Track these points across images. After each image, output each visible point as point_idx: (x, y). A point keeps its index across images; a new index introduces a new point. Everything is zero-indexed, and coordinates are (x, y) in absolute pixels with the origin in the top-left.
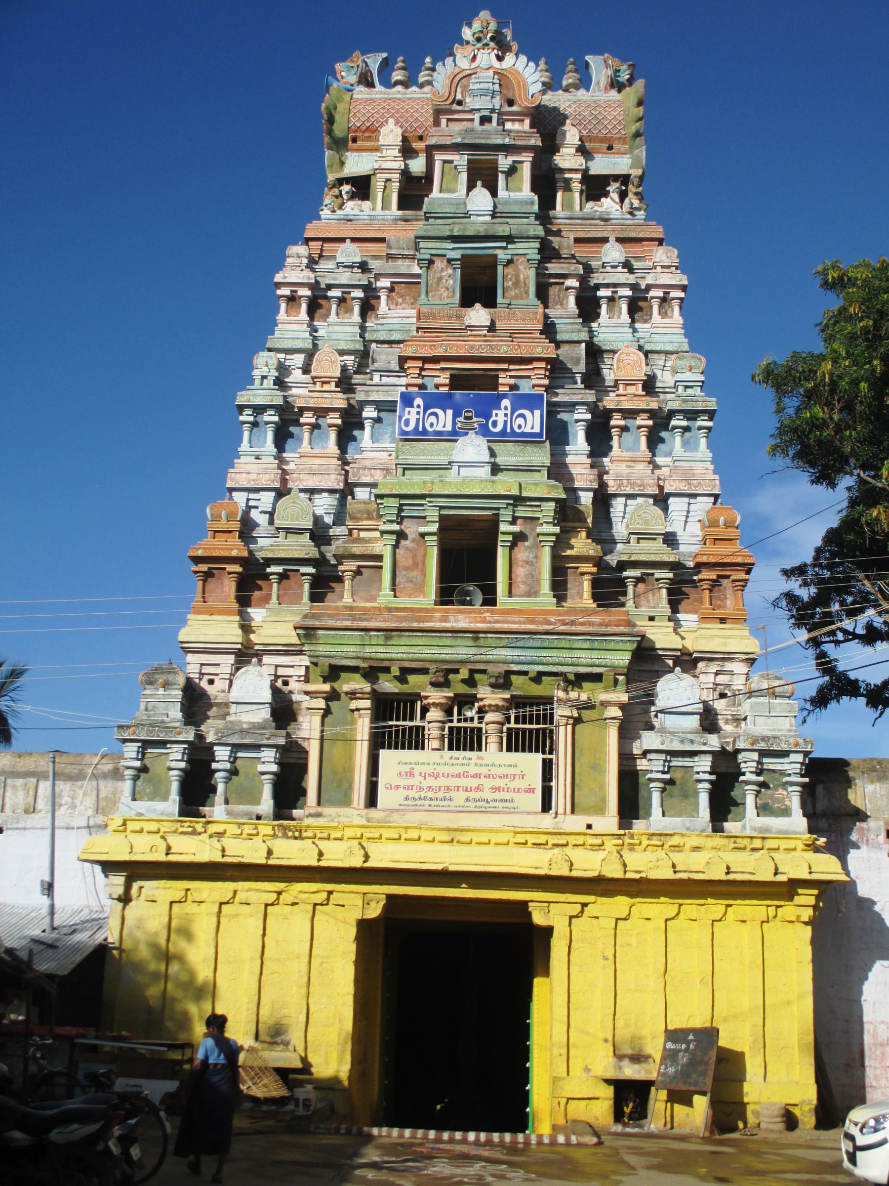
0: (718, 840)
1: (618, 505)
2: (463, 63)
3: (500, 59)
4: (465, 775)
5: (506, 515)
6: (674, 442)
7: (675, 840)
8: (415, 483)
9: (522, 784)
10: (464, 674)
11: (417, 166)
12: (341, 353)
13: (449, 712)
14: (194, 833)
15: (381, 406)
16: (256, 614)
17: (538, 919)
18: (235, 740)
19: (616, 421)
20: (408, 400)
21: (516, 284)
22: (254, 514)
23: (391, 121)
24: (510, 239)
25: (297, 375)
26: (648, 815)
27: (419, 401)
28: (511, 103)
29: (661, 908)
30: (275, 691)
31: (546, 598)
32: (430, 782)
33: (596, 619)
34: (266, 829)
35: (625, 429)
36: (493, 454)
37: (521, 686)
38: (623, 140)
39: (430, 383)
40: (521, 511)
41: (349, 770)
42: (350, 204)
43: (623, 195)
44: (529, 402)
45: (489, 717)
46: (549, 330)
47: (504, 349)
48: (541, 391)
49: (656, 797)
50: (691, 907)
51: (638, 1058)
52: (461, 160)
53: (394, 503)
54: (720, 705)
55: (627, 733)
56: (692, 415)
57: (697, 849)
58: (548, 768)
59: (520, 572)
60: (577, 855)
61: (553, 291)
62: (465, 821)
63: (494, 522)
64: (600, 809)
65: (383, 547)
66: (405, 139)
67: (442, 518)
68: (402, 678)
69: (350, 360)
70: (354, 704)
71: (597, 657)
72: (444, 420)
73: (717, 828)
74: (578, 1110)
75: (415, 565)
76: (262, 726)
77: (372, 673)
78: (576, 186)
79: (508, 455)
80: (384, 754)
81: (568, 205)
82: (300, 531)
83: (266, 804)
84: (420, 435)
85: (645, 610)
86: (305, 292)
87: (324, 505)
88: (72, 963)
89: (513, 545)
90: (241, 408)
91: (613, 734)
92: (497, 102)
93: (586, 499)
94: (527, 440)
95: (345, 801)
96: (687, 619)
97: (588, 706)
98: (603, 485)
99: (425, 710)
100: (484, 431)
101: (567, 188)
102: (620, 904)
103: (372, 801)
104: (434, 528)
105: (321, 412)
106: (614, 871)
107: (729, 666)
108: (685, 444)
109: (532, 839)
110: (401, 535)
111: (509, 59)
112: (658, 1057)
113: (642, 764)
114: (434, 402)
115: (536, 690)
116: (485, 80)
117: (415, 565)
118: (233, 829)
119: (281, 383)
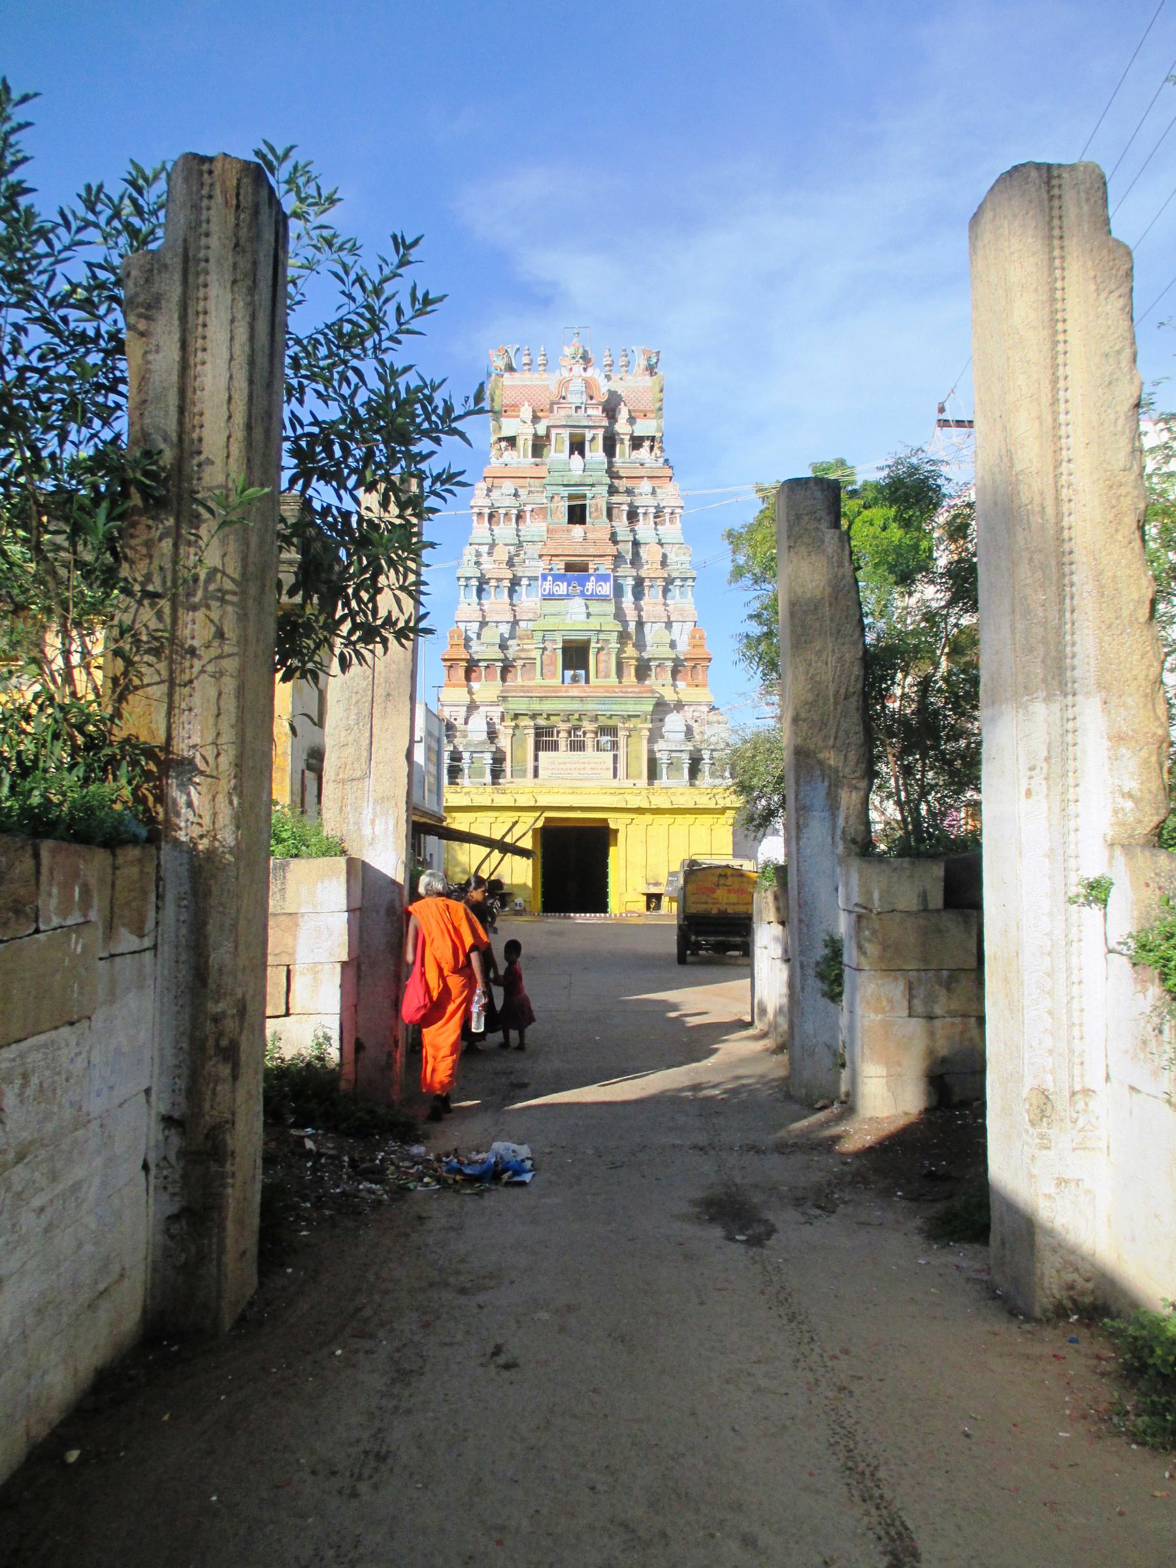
0: (693, 790)
1: (647, 628)
2: (566, 374)
3: (585, 370)
4: (578, 763)
5: (594, 639)
6: (675, 591)
7: (673, 790)
8: (549, 623)
9: (605, 766)
10: (576, 716)
11: (542, 431)
12: (506, 545)
13: (569, 733)
14: (456, 792)
15: (530, 578)
16: (475, 685)
17: (612, 826)
18: (472, 749)
19: (647, 583)
20: (544, 577)
21: (596, 510)
22: (469, 633)
23: (526, 404)
24: (593, 485)
25: (485, 558)
26: (661, 778)
27: (550, 578)
28: (591, 398)
29: (667, 819)
30: (488, 723)
31: (613, 679)
32: (562, 766)
33: (637, 690)
34: (489, 789)
35: (652, 586)
36: (587, 607)
37: (603, 721)
38: (652, 412)
39: (555, 567)
40: (602, 636)
41: (525, 761)
42: (506, 453)
43: (652, 448)
44: (603, 578)
45: (588, 735)
46: (614, 539)
47: (591, 551)
48: (609, 572)
49: (664, 771)
50: (680, 818)
51: (656, 884)
52: (565, 434)
53: (541, 634)
54: (695, 725)
55: (651, 740)
56: (684, 579)
57: (682, 794)
58: (615, 757)
59: (602, 666)
60: (628, 797)
61: (615, 512)
62: (578, 784)
63: (588, 642)
64: (639, 776)
65: (536, 654)
66: (534, 411)
67: (564, 642)
68: (548, 718)
69: (512, 549)
70: (526, 731)
71: (638, 707)
72: (562, 588)
73: (692, 785)
74: (630, 907)
75: (552, 663)
76: (483, 743)
77: (534, 717)
78: (627, 443)
79: (595, 607)
80: (541, 754)
81: (622, 455)
82: (494, 645)
83: (488, 778)
84: (549, 597)
85: (660, 682)
86: (487, 511)
87: (505, 629)
88: (760, 912)
89: (598, 653)
90: (459, 579)
91: (645, 743)
92: (584, 398)
93: (632, 627)
94: (604, 599)
95: (523, 773)
96: (681, 684)
97: (635, 729)
98: (640, 617)
99: (558, 732)
100: (582, 594)
101: (622, 441)
102: (648, 817)
103: (536, 775)
104: (560, 645)
105: (499, 580)
106: (645, 805)
107: (699, 708)
108: (681, 593)
109: (609, 791)
110: (544, 649)
111: (590, 371)
112: (665, 883)
113: (658, 755)
114: (557, 578)
115: (610, 723)
116: (577, 385)
117: (552, 663)
118: (474, 790)
119: (478, 563)
